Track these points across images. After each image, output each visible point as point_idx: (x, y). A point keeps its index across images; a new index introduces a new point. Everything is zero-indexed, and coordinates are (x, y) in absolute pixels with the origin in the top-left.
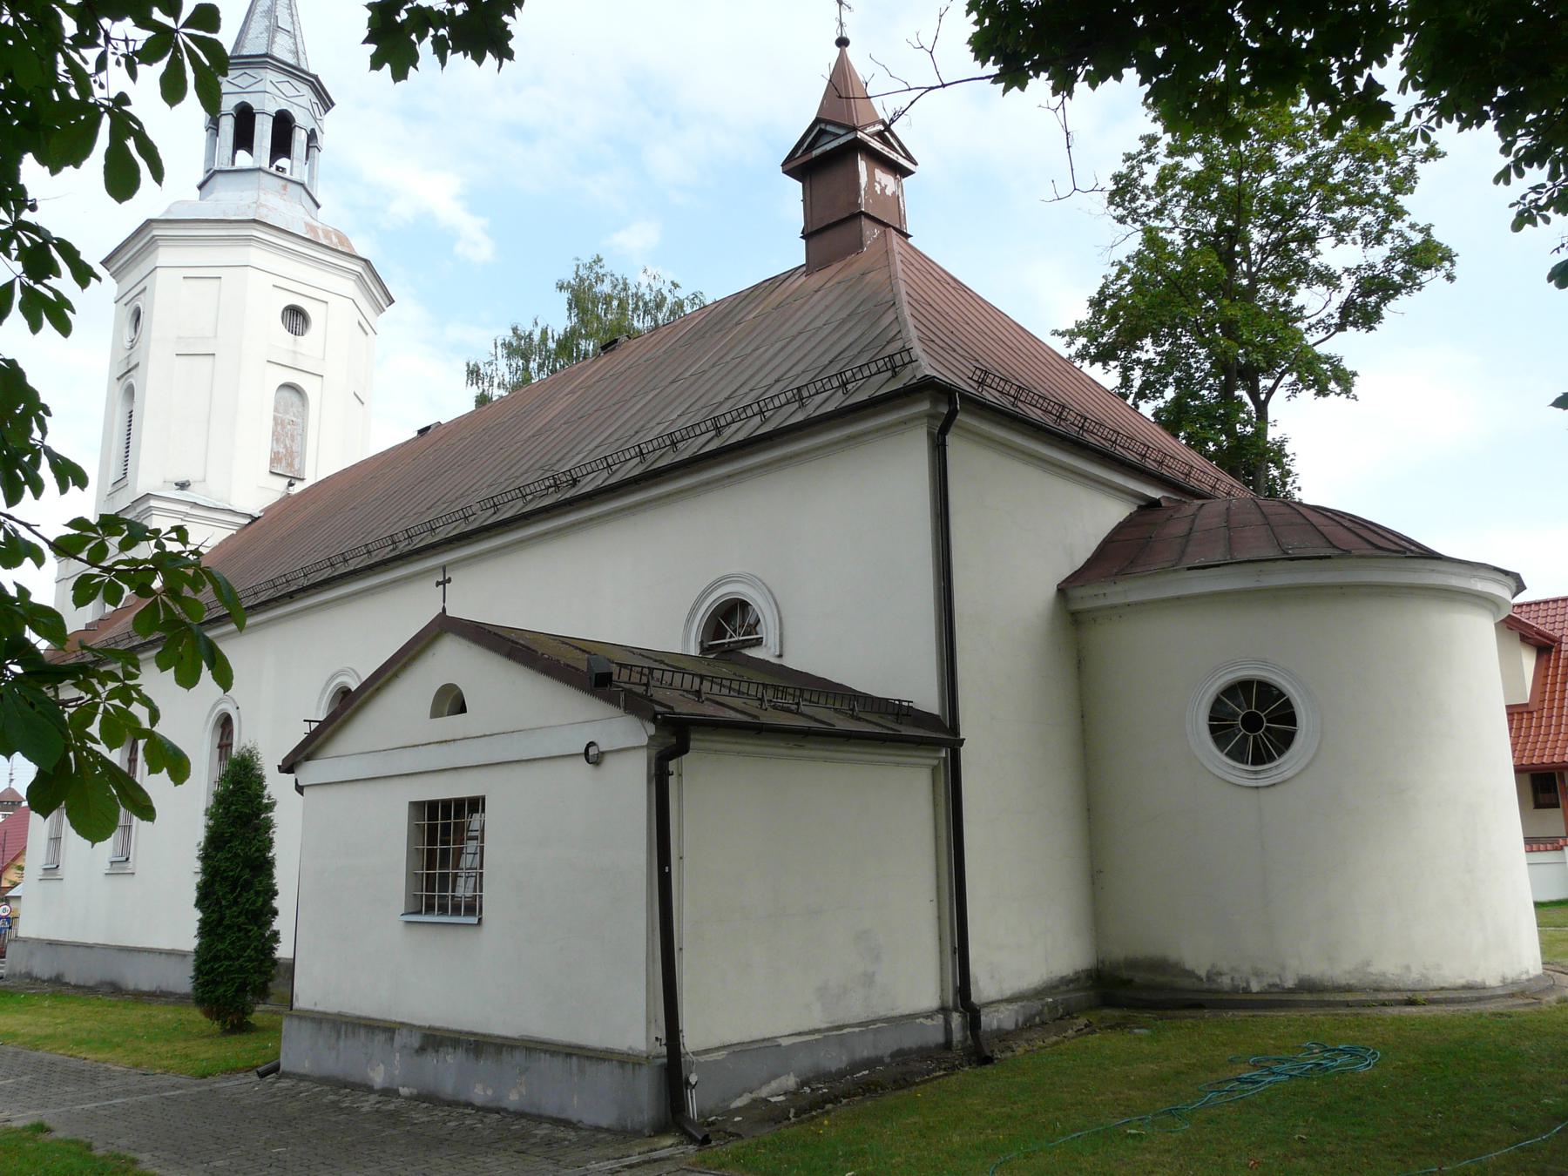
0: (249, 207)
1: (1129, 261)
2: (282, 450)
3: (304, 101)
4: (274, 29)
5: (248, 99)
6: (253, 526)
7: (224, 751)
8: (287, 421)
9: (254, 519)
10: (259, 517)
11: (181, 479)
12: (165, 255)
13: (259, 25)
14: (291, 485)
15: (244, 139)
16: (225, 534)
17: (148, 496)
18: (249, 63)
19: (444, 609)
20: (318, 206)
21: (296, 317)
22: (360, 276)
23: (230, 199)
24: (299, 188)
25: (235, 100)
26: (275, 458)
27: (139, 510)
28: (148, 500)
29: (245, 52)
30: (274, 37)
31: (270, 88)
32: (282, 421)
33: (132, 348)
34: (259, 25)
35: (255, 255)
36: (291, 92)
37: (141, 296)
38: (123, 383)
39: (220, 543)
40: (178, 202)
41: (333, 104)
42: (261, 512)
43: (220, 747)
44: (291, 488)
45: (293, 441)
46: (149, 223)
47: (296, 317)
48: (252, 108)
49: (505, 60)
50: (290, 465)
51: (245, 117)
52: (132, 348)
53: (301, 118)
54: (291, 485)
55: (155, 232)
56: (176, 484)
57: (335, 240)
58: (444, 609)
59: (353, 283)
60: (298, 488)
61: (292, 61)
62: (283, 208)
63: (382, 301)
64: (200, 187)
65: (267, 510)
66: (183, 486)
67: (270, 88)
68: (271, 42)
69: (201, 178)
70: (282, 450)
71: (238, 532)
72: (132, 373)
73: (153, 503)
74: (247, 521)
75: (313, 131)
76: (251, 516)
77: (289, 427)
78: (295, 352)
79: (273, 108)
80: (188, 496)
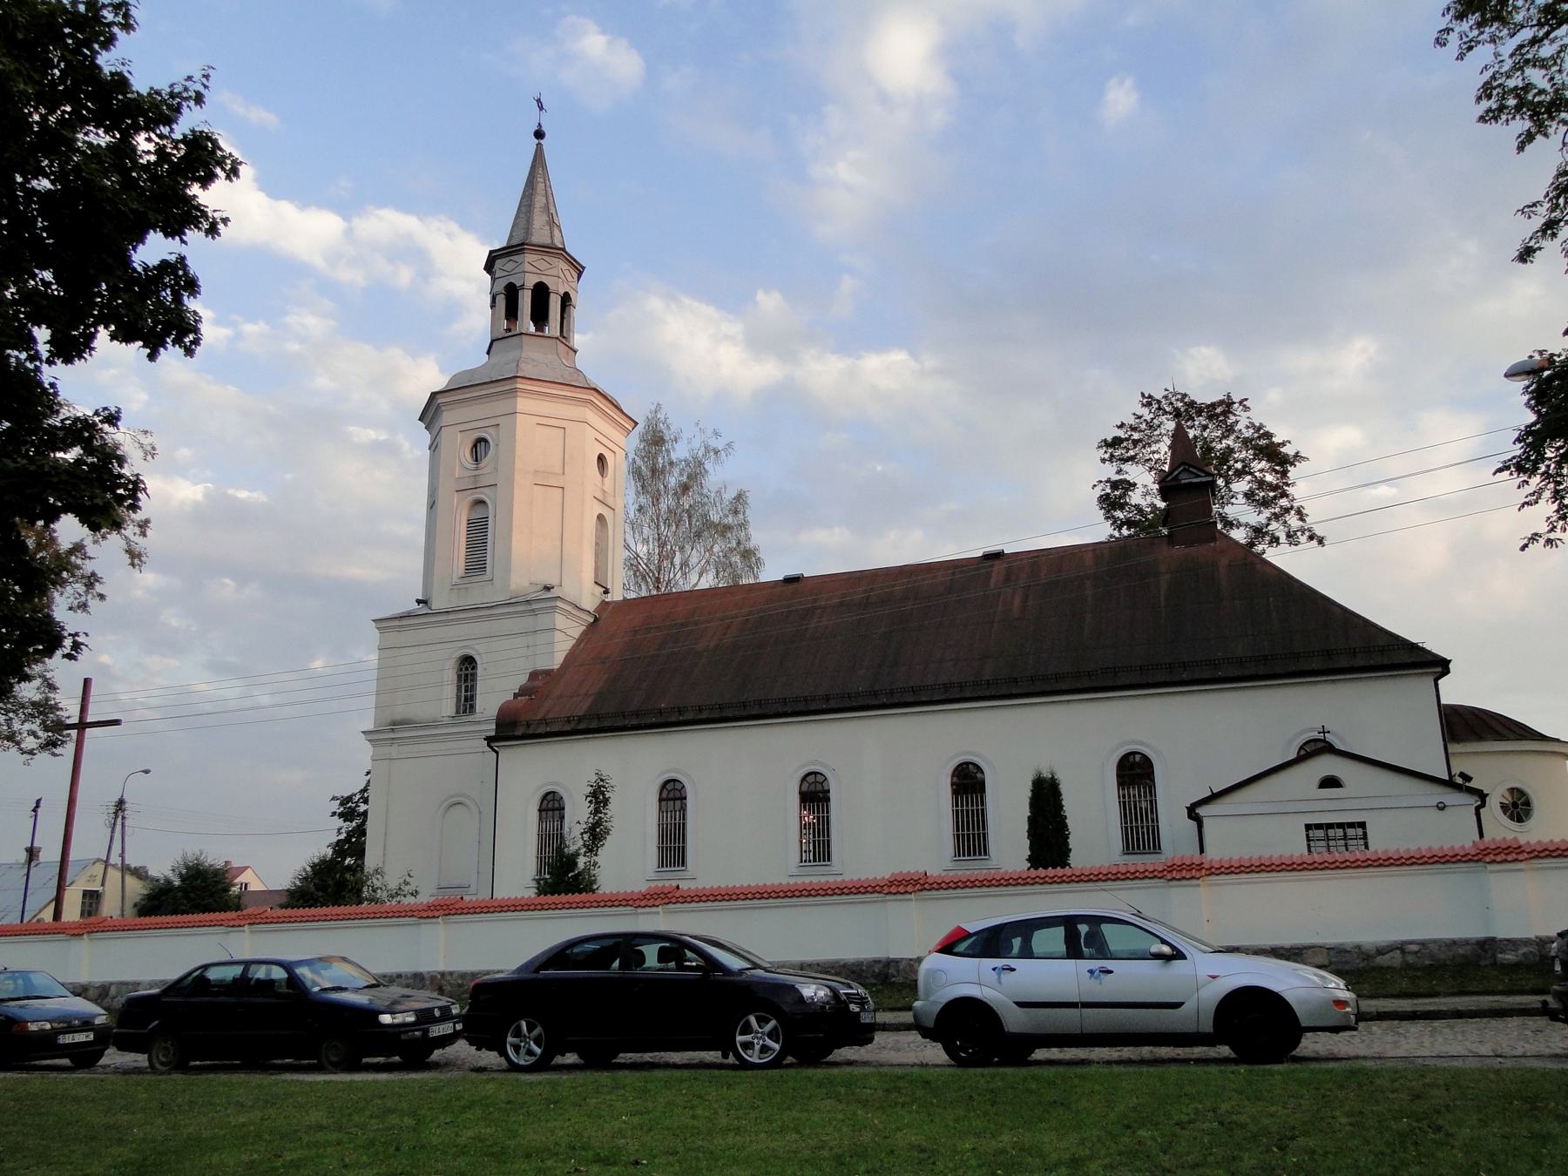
18: (572, 264)
24: (495, 343)
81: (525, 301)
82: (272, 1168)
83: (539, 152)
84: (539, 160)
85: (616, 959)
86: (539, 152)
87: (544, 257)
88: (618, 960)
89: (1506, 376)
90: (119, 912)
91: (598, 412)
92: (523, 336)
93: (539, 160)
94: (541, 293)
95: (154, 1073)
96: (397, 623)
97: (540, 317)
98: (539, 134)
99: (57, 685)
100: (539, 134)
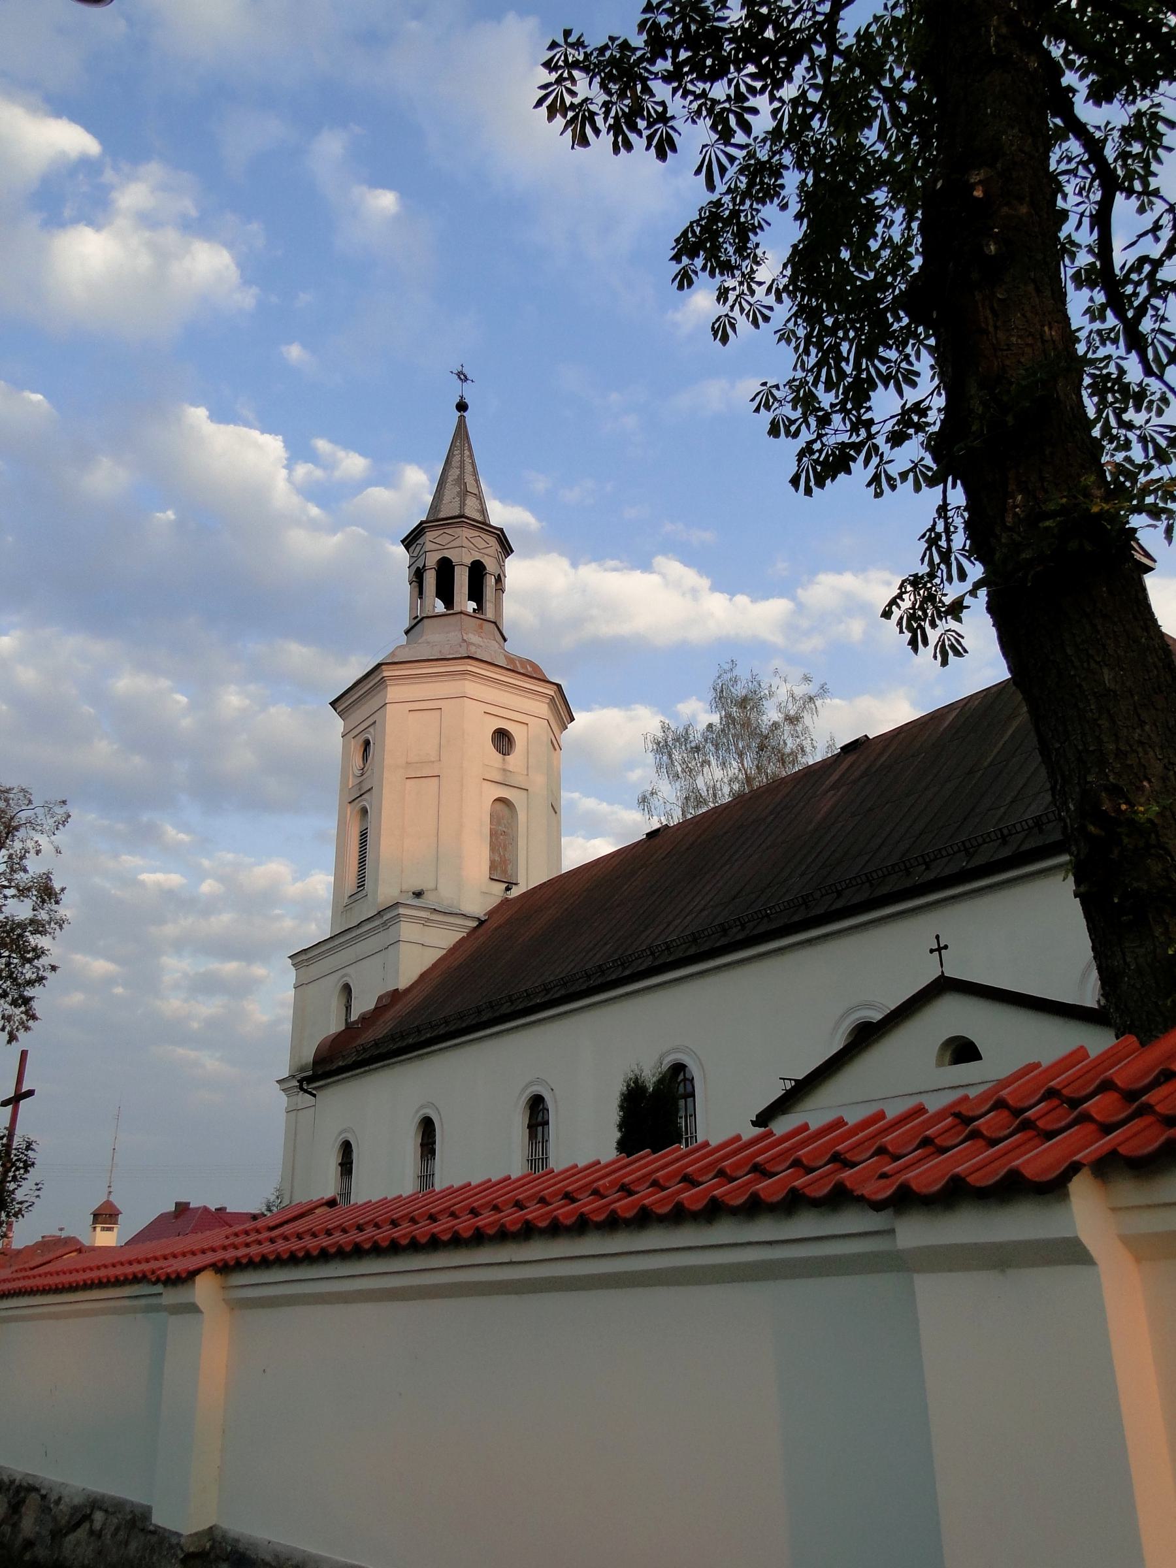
0: (461, 646)
1: (679, 261)
2: (497, 858)
3: (492, 551)
4: (464, 493)
5: (447, 554)
6: (481, 931)
7: (344, 1167)
8: (499, 832)
9: (481, 923)
10: (486, 920)
11: (418, 889)
12: (393, 692)
13: (451, 492)
14: (508, 889)
15: (445, 592)
16: (456, 936)
17: (397, 905)
18: (448, 524)
19: (942, 972)
20: (505, 640)
21: (503, 739)
22: (552, 699)
23: (437, 638)
24: (493, 625)
25: (437, 556)
26: (493, 867)
27: (385, 918)
28: (398, 907)
29: (442, 515)
30: (465, 500)
31: (466, 543)
32: (496, 833)
33: (362, 775)
34: (451, 492)
35: (471, 687)
36: (482, 544)
37: (371, 730)
38: (358, 805)
39: (454, 945)
40: (398, 647)
41: (512, 551)
42: (485, 915)
43: (529, 1127)
44: (508, 893)
45: (506, 850)
46: (379, 666)
47: (503, 739)
48: (452, 562)
49: (964, 605)
50: (505, 872)
51: (445, 568)
52: (362, 775)
53: (490, 565)
54: (508, 889)
55: (385, 674)
56: (414, 893)
57: (530, 669)
58: (942, 972)
59: (547, 705)
60: (515, 892)
61: (480, 519)
62: (480, 642)
63: (565, 718)
64: (407, 632)
65: (491, 913)
66: (418, 894)
67: (466, 543)
68: (463, 504)
69: (407, 626)
70: (497, 858)
71: (469, 935)
72: (363, 797)
73: (402, 911)
74: (475, 924)
75: (499, 575)
76: (479, 919)
77: (501, 837)
78: (504, 770)
79: (468, 561)
80: (422, 903)
81: (430, 579)
82: (747, 782)
83: (461, 425)
84: (461, 433)
85: (1064, 123)
86: (461, 425)
87: (445, 531)
88: (1062, 125)
89: (1170, 543)
90: (719, 721)
91: (511, 690)
92: (425, 620)
93: (461, 433)
94: (477, 571)
95: (282, 1234)
96: (304, 957)
97: (476, 593)
98: (462, 407)
99: (38, 1015)
100: (462, 407)
